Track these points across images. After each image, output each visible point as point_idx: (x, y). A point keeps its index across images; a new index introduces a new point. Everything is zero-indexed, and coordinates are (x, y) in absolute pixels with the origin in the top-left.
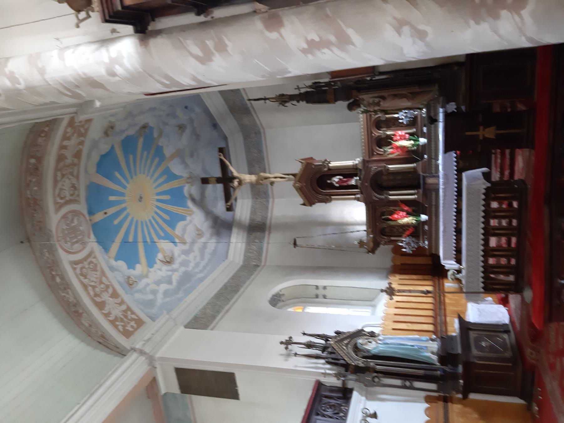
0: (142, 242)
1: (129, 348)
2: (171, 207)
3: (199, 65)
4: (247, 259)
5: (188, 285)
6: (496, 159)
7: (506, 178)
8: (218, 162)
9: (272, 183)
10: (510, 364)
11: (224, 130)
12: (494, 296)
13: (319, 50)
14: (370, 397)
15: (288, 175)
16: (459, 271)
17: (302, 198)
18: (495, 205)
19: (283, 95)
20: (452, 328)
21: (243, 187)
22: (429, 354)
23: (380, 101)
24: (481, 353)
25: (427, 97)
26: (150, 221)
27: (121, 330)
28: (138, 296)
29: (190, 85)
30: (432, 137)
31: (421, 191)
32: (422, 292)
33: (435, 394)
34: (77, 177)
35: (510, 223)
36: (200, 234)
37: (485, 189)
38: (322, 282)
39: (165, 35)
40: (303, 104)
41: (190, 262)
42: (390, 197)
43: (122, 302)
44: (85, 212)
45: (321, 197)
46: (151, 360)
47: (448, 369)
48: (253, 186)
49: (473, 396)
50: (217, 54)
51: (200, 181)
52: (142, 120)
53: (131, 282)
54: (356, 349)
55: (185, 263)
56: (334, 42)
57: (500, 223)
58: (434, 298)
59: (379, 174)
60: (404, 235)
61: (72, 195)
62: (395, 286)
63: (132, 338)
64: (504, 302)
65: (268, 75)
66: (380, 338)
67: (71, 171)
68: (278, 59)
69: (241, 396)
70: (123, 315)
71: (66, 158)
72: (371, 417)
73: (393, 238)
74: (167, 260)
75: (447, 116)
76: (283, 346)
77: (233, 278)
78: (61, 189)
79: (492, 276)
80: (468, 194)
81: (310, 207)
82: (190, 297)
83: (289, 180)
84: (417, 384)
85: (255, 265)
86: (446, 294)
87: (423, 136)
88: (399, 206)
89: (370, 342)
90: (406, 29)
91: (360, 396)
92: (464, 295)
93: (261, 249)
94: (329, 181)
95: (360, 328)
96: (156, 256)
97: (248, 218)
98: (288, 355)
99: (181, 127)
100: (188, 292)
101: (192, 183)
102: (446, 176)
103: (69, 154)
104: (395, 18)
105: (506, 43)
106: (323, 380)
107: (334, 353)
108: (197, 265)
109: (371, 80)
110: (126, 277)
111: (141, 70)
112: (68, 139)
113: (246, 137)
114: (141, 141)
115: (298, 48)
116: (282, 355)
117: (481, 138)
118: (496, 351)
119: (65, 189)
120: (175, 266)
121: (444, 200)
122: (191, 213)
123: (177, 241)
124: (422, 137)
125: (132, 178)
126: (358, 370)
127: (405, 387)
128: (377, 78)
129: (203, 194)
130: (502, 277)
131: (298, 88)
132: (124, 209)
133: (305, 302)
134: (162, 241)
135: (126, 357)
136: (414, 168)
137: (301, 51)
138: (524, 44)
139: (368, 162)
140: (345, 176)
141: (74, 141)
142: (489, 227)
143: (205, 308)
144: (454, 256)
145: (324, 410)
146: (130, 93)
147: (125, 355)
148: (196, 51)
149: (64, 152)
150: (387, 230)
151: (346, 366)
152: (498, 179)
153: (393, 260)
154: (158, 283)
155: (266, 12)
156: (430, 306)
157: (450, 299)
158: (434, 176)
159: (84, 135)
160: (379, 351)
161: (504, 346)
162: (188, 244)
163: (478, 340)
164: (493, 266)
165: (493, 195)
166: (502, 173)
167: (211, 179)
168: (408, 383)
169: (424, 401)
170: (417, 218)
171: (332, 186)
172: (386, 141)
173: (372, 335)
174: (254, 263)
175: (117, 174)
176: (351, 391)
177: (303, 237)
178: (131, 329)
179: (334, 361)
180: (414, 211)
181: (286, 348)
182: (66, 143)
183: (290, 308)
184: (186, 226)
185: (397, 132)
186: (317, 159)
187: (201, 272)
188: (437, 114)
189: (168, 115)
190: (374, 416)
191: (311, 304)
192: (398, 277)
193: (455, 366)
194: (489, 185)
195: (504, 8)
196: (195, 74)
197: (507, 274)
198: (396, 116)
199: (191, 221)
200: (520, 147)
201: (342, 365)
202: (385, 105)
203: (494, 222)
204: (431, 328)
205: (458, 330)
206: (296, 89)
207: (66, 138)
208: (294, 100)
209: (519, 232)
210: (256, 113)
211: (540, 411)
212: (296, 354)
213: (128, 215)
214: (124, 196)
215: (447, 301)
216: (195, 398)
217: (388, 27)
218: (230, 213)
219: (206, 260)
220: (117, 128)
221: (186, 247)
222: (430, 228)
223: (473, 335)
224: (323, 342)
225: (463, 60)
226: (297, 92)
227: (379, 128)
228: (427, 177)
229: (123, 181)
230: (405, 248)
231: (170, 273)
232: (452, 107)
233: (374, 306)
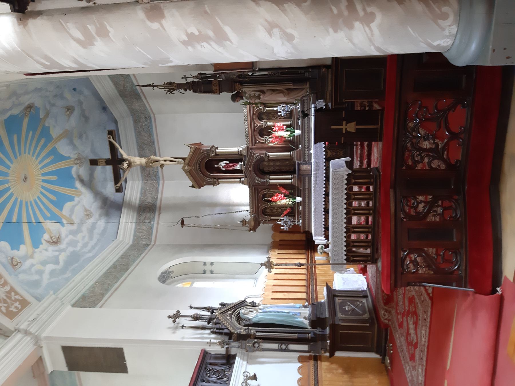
0: (22, 223)
1: (13, 329)
2: (70, 190)
3: (80, 48)
4: (136, 238)
5: (76, 265)
6: (357, 151)
7: (365, 166)
8: (108, 143)
9: (162, 166)
10: (368, 325)
11: (114, 114)
12: (356, 266)
13: (199, 43)
14: (250, 361)
15: (178, 158)
16: (327, 246)
17: (191, 180)
18: (356, 189)
19: (171, 83)
20: (321, 295)
21: (133, 169)
22: (302, 319)
23: (260, 95)
24: (344, 316)
25: (302, 93)
26: (35, 201)
27: (4, 311)
28: (22, 276)
29: (71, 67)
30: (305, 129)
31: (296, 176)
32: (296, 264)
33: (307, 354)
35: (368, 204)
36: (88, 215)
37: (347, 175)
38: (209, 259)
39: (45, 17)
40: (189, 92)
41: (78, 242)
42: (271, 181)
43: (5, 283)
45: (209, 180)
46: (37, 340)
47: (318, 331)
48: (144, 168)
49: (338, 354)
50: (98, 39)
51: (89, 163)
52: (27, 100)
53: (15, 263)
54: (239, 319)
55: (72, 243)
56: (212, 37)
57: (360, 204)
58: (308, 269)
59: (261, 160)
60: (283, 215)
62: (274, 260)
63: (17, 319)
64: (364, 271)
65: (150, 63)
66: (260, 307)
68: (159, 48)
69: (129, 370)
70: (6, 296)
72: (252, 379)
73: (272, 218)
74: (54, 240)
75: (316, 111)
76: (171, 320)
77: (122, 257)
79: (354, 249)
80: (334, 179)
81: (198, 189)
82: (78, 277)
83: (179, 163)
84: (292, 347)
85: (145, 245)
86: (317, 266)
87: (298, 128)
88: (278, 189)
89: (252, 312)
90: (276, 31)
91: (241, 361)
92: (331, 266)
93: (151, 228)
94: (216, 166)
95: (243, 299)
96: (42, 237)
97: (138, 199)
98: (176, 328)
99: (70, 109)
100: (75, 272)
101: (80, 164)
102: (316, 163)
104: (266, 20)
105: (359, 51)
106: (208, 348)
107: (219, 323)
108: (85, 245)
109: (252, 75)
110: (9, 258)
113: (136, 121)
114: (26, 121)
115: (179, 40)
116: (169, 328)
117: (344, 131)
118: (358, 314)
120: (62, 246)
121: (315, 184)
122: (80, 194)
123: (64, 221)
124: (297, 129)
125: (16, 157)
126: (241, 338)
127: (281, 350)
128: (258, 73)
129: (91, 175)
130: (361, 250)
131: (185, 77)
133: (194, 278)
134: (48, 221)
135: (10, 338)
136: (291, 156)
137: (181, 42)
138: (374, 52)
139: (251, 149)
140: (231, 161)
142: (351, 208)
143: (93, 287)
144: (324, 233)
145: (209, 377)
146: (7, 72)
147: (9, 337)
148: (78, 34)
150: (268, 210)
151: (230, 335)
152: (358, 167)
153: (273, 236)
154: (44, 263)
155: (149, 2)
156: (304, 277)
157: (321, 270)
158: (307, 164)
160: (259, 319)
161: (363, 308)
162: (75, 224)
163: (342, 305)
164: (354, 241)
165: (353, 181)
166: (361, 162)
167: (100, 161)
168: (284, 347)
169: (297, 361)
170: (292, 200)
171: (219, 170)
172: (266, 131)
173: (254, 305)
174: (144, 243)
176: (234, 357)
177: (190, 217)
178: (15, 310)
179: (218, 331)
180: (290, 193)
181: (174, 322)
183: (179, 284)
184: (74, 206)
185: (277, 123)
186: (205, 145)
187: (90, 251)
188: (309, 109)
189: (56, 96)
190: (254, 377)
191: (198, 280)
192: (277, 251)
193: (324, 328)
194: (350, 172)
195: (357, 20)
196: (76, 57)
197: (366, 247)
198: (275, 109)
199: (79, 202)
200: (376, 141)
201: (226, 334)
202: (265, 98)
203: (355, 203)
204: (304, 296)
205: (326, 297)
206: (182, 78)
208: (180, 88)
209: (374, 212)
211: (391, 363)
212: (183, 327)
213: (11, 195)
215: (318, 272)
216: (84, 375)
217: (261, 28)
218: (119, 194)
219: (95, 240)
221: (74, 227)
222: (304, 208)
223: (338, 300)
224: (209, 314)
225: (329, 63)
226: (184, 81)
227: (261, 119)
228: (301, 164)
229: (8, 162)
230: (284, 226)
231: (57, 253)
232: (321, 104)
233: (256, 279)
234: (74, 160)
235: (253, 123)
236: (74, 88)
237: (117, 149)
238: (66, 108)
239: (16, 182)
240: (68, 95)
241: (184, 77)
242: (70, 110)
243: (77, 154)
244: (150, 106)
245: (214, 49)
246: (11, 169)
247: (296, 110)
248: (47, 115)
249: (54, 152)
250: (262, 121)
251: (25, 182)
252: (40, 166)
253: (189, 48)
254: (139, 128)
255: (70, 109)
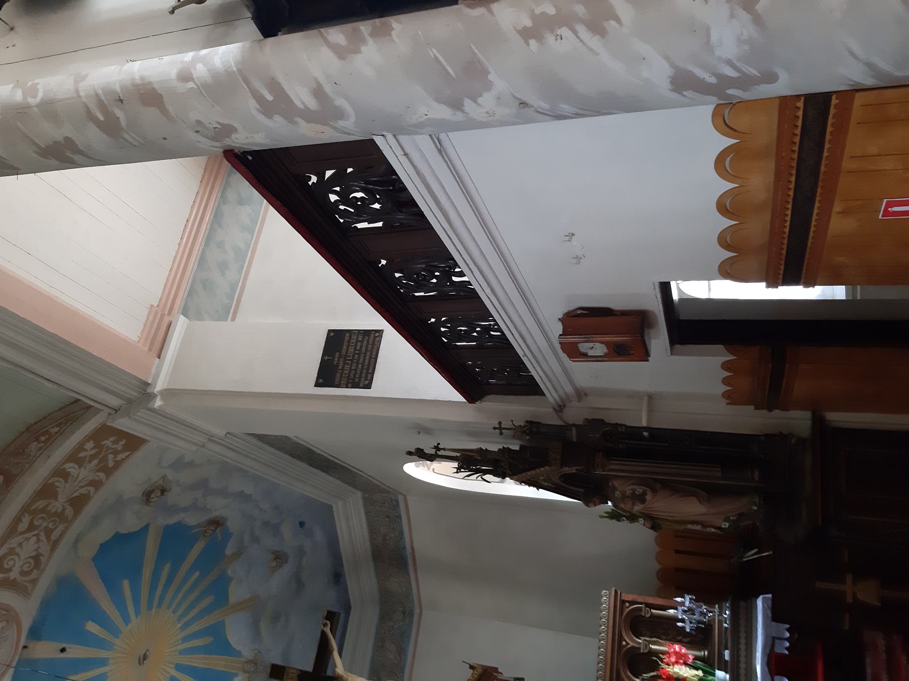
8: (319, 634)
13: (552, 31)
23: (644, 494)
34: (55, 545)
44: (26, 624)
50: (370, 41)
52: (219, 507)
61: (23, 573)
67: (50, 526)
71: (56, 499)
78: (12, 551)
99: (279, 558)
103: (65, 491)
111: (235, 69)
112: (80, 462)
113: (385, 616)
117: (849, 599)
119: (18, 555)
124: (719, 669)
125: (150, 607)
132: (103, 662)
137: (519, 32)
141: (85, 473)
149: (59, 482)
159: (109, 472)
175: (126, 584)
182: (71, 467)
196: (322, 79)
206: (495, 428)
207: (74, 457)
210: (415, 571)
214: (117, 638)
220: (172, 497)
234: (246, 662)
235: (617, 639)
236: (302, 520)
237: (331, 652)
238: (274, 554)
239: (125, 655)
240: (287, 530)
241: (498, 426)
242: (278, 560)
243: (256, 651)
244: (418, 587)
245: (581, 41)
246: (129, 624)
247: (720, 623)
248: (238, 554)
249: (217, 633)
250: (640, 639)
251: (140, 664)
252: (180, 647)
253: (532, 42)
254: (385, 633)
255: (280, 559)
